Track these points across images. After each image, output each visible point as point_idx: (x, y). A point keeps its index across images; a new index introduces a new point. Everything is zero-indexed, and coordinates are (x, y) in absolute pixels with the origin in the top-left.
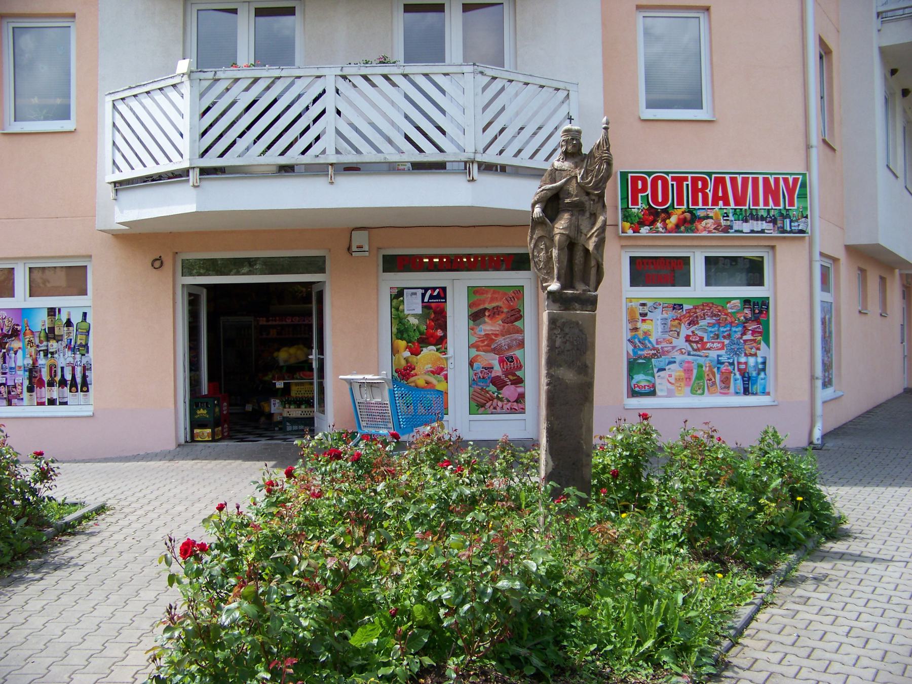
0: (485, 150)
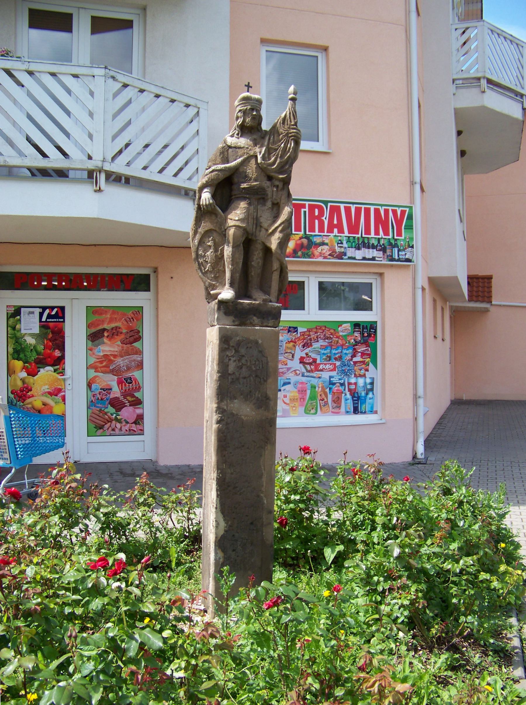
0: (114, 158)
